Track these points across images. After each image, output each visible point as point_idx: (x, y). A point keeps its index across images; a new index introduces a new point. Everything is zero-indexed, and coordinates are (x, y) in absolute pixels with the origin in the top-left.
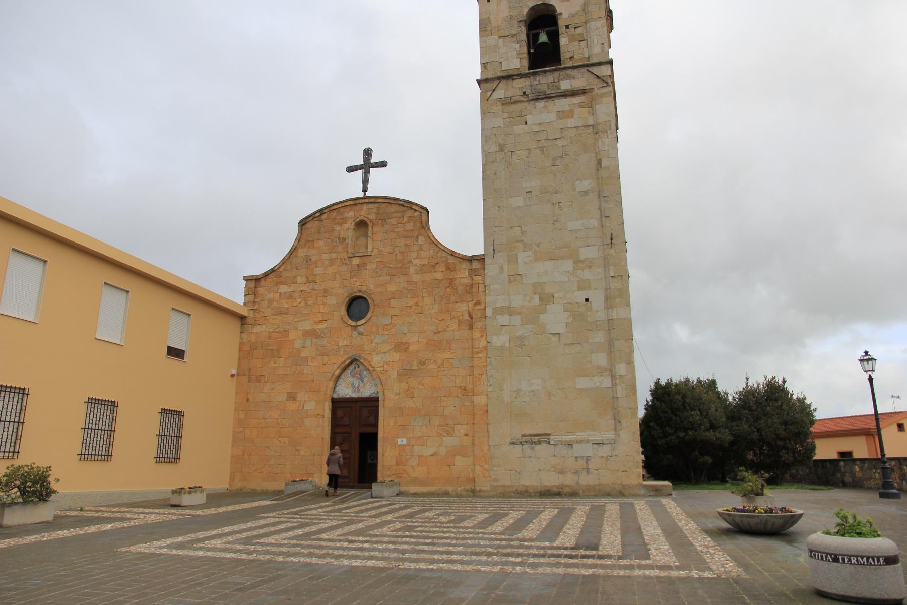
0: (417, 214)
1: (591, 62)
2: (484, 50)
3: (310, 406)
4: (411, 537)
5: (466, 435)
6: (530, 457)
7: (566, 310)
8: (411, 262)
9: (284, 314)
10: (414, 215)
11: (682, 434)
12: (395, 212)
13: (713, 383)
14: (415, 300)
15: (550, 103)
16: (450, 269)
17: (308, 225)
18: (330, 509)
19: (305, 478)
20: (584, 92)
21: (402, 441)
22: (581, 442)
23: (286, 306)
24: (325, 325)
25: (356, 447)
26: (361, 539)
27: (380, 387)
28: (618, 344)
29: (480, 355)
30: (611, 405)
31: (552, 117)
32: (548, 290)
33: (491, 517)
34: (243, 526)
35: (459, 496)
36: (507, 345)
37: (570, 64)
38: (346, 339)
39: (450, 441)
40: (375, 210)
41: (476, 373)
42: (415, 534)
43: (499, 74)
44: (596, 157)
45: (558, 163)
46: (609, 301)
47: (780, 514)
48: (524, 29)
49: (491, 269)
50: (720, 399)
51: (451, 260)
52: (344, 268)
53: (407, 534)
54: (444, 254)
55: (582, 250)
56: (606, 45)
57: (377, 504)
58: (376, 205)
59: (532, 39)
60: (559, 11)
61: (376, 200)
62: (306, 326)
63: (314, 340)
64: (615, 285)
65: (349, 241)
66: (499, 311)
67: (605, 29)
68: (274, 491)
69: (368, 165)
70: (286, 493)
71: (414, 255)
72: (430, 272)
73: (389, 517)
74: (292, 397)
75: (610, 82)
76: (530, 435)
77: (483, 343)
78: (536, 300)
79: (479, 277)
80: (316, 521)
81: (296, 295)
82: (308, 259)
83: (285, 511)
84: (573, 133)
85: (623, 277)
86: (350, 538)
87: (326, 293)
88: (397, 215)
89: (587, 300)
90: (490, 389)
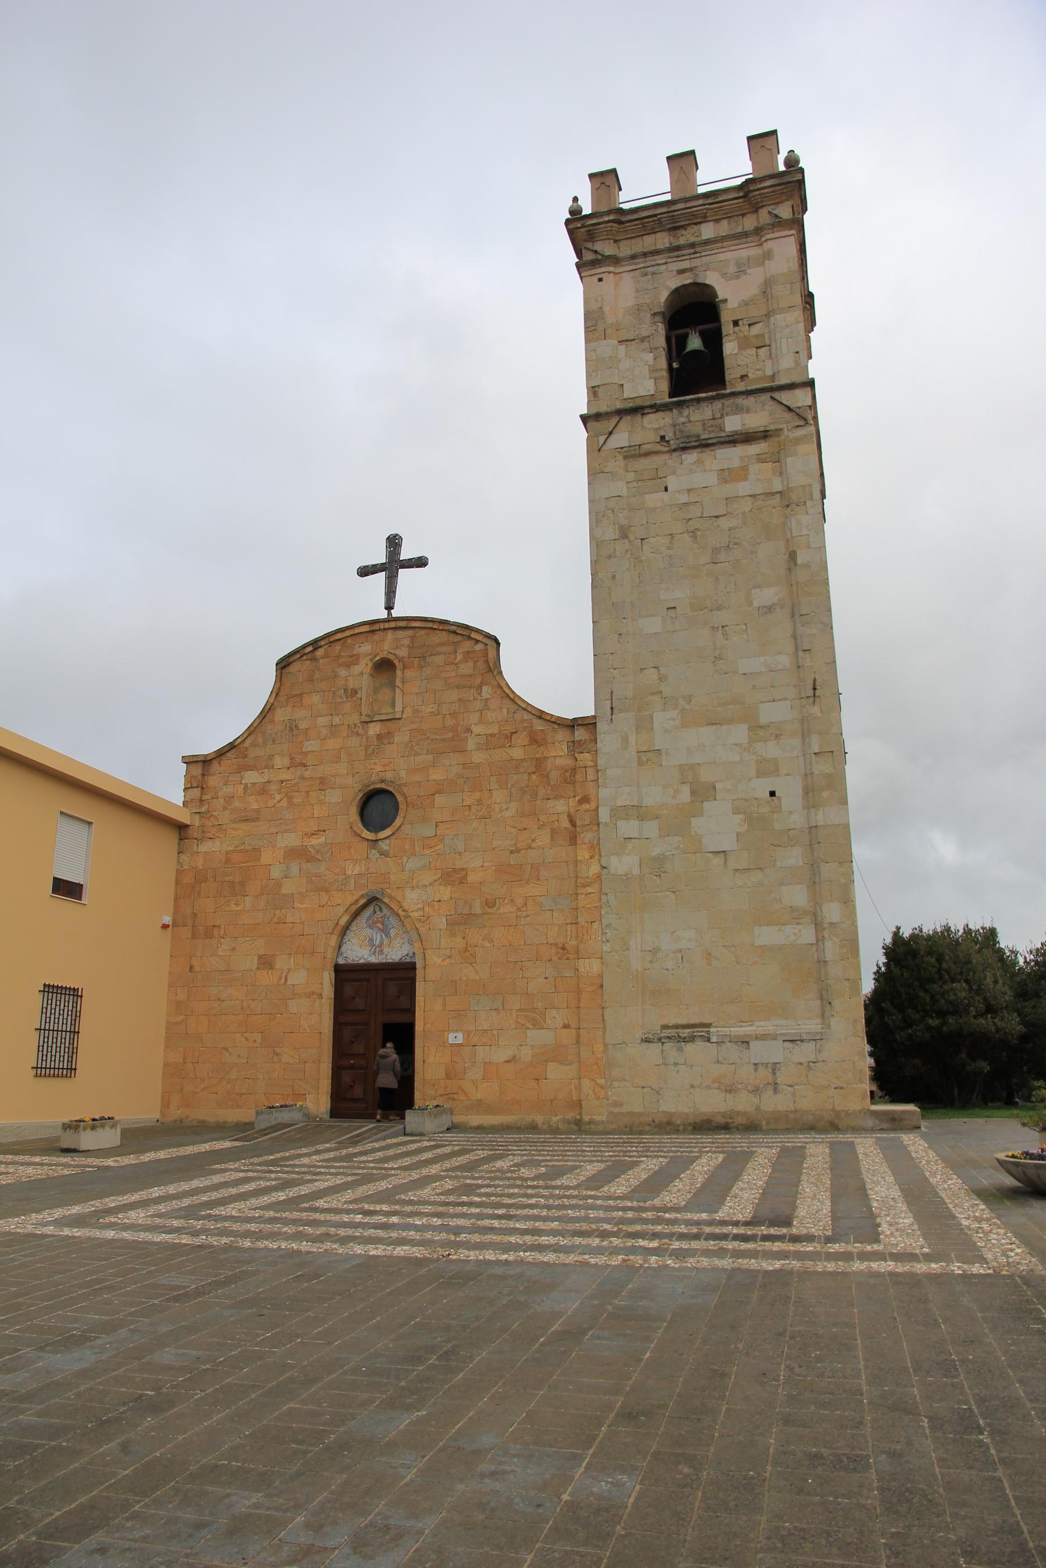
0: (479, 647)
1: (777, 383)
2: (593, 364)
4: (471, 1204)
5: (566, 1026)
6: (676, 1064)
7: (736, 811)
8: (469, 730)
9: (253, 820)
10: (472, 649)
12: (442, 644)
13: (991, 934)
15: (707, 455)
17: (293, 668)
18: (332, 1155)
19: (289, 1102)
21: (455, 1038)
22: (762, 1037)
23: (255, 806)
24: (323, 839)
27: (417, 945)
28: (827, 870)
29: (589, 890)
31: (712, 479)
34: (185, 1186)
35: (555, 1131)
36: (636, 871)
37: (741, 387)
38: (358, 864)
39: (537, 1037)
40: (407, 642)
41: (581, 920)
42: (477, 1199)
43: (619, 406)
45: (722, 557)
49: (607, 741)
50: (1003, 960)
51: (539, 725)
52: (355, 741)
53: (465, 1198)
56: (803, 354)
58: (410, 633)
59: (675, 346)
60: (721, 295)
61: (408, 623)
62: (291, 840)
64: (821, 767)
66: (622, 812)
67: (801, 327)
69: (394, 563)
70: (257, 1128)
71: (474, 717)
73: (434, 1169)
74: (266, 962)
76: (677, 1027)
77: (594, 869)
81: (273, 787)
82: (292, 727)
83: (256, 1160)
84: (747, 506)
85: (836, 753)
86: (366, 1206)
87: (323, 783)
88: (445, 649)
89: (772, 794)
90: (606, 948)
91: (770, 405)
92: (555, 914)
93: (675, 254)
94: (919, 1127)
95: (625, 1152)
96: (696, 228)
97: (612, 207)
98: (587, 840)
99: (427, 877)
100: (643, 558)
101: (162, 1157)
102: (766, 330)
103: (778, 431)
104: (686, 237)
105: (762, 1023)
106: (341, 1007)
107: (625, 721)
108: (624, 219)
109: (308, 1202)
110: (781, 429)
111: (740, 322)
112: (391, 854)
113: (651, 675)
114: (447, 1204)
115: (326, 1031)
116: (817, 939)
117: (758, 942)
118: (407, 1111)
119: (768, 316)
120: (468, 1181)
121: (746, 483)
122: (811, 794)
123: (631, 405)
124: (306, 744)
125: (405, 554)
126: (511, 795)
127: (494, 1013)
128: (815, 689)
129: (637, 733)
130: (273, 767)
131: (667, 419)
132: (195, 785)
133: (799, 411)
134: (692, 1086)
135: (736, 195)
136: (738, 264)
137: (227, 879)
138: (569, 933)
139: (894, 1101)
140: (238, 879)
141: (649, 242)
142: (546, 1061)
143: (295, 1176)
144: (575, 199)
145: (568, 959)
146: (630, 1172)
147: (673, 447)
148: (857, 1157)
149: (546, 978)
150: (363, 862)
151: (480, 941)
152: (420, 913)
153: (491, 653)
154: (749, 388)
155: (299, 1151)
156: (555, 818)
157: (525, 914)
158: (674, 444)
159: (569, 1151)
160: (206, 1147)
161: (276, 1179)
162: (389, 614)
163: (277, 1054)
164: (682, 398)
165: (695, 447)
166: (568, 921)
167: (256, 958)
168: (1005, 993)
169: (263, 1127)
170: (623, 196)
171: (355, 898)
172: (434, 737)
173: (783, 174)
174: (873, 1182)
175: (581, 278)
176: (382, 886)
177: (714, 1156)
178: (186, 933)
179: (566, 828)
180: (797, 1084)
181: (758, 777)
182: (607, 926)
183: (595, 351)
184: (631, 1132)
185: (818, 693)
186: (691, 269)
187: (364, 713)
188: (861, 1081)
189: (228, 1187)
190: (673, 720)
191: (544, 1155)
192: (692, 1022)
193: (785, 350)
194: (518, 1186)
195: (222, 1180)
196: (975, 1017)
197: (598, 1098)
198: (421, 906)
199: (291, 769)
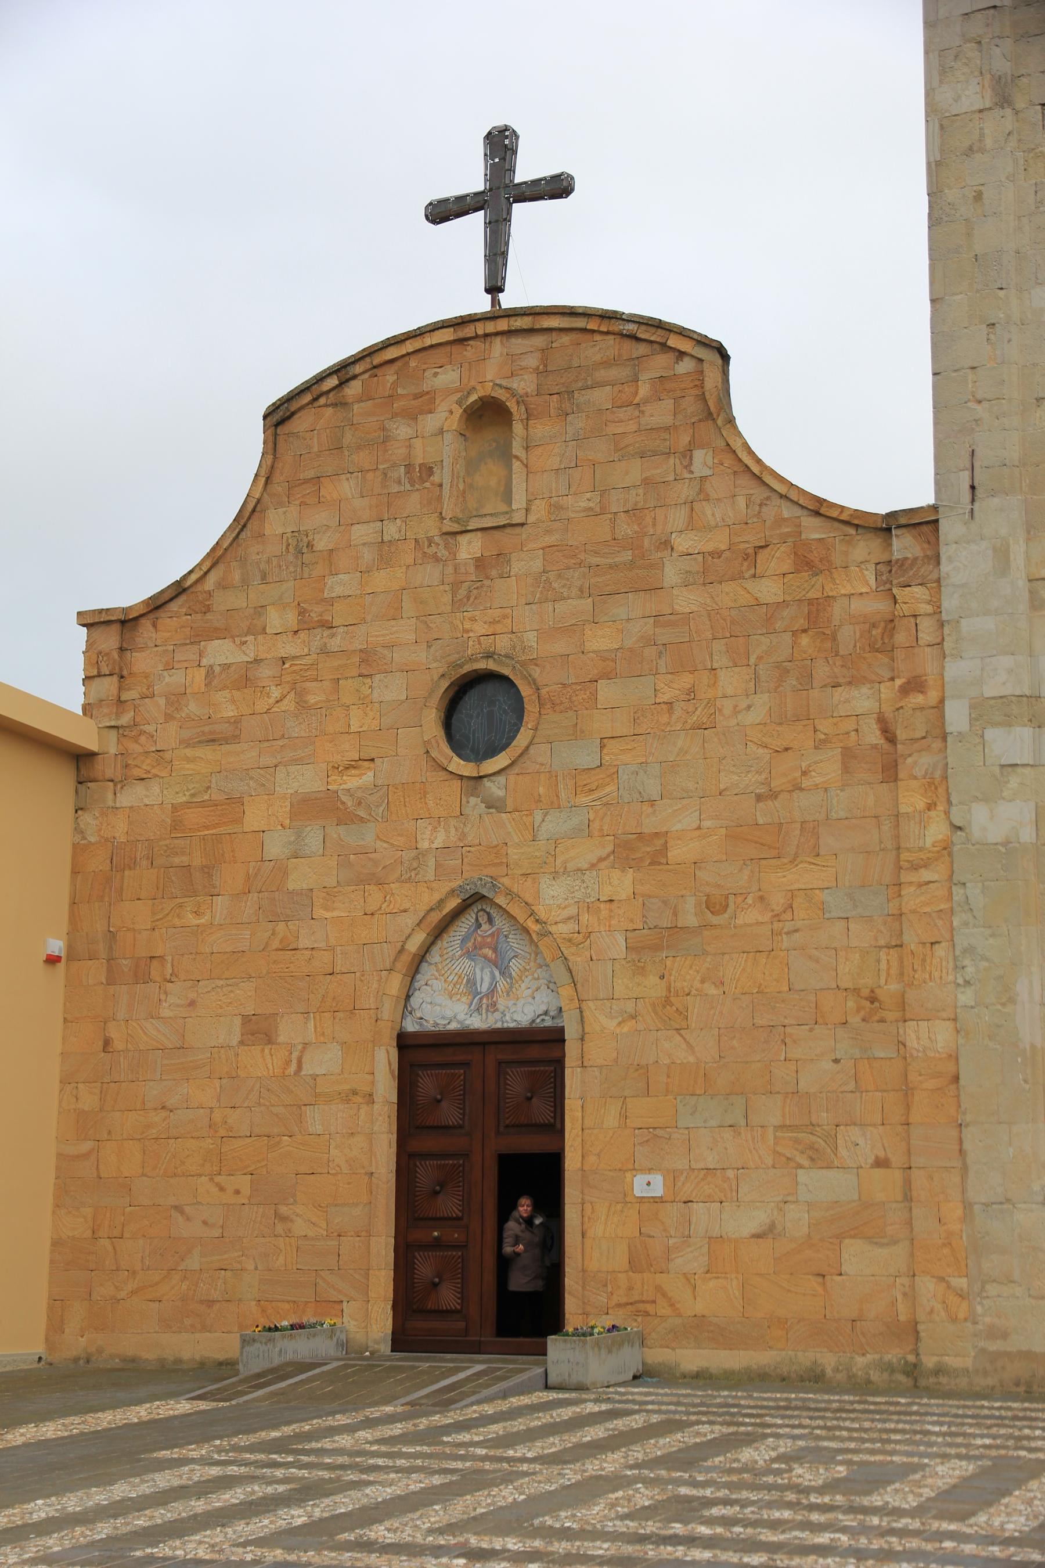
0: (685, 366)
3: (324, 1062)
4: (691, 1541)
5: (881, 1163)
8: (666, 545)
9: (226, 741)
10: (679, 370)
12: (606, 364)
14: (686, 680)
16: (809, 565)
17: (300, 424)
18: (397, 1429)
19: (308, 1318)
21: (648, 1185)
23: (230, 712)
24: (368, 777)
25: (484, 1211)
26: (512, 1544)
27: (567, 992)
29: (926, 875)
33: (983, 1472)
34: (99, 1497)
35: (862, 1387)
36: (1027, 835)
38: (444, 827)
39: (821, 1185)
40: (532, 361)
42: (704, 1530)
49: (963, 560)
51: (814, 530)
52: (429, 574)
53: (678, 1528)
54: (787, 511)
57: (566, 1413)
58: (539, 341)
61: (535, 321)
62: (306, 780)
63: (333, 832)
65: (443, 475)
66: (992, 711)
68: (202, 1364)
69: (502, 191)
70: (244, 1372)
71: (678, 517)
73: (610, 1463)
74: (259, 1030)
77: (936, 831)
80: (352, 1476)
81: (265, 672)
82: (301, 546)
83: (243, 1440)
86: (473, 1541)
87: (368, 663)
88: (613, 373)
90: (966, 997)
92: (852, 926)
95: (1020, 1438)
98: (919, 772)
99: (586, 852)
101: (50, 1435)
106: (412, 1119)
107: (1002, 515)
109: (352, 1530)
114: (643, 1539)
115: (383, 1171)
118: (551, 1339)
120: (684, 1490)
124: (330, 581)
125: (525, 171)
126: (756, 677)
127: (728, 1134)
129: (1028, 540)
130: (264, 631)
132: (105, 670)
137: (177, 860)
138: (883, 965)
140: (198, 861)
142: (840, 1237)
143: (326, 1474)
145: (882, 1021)
146: (1033, 1484)
149: (836, 1061)
150: (453, 822)
151: (697, 984)
152: (572, 926)
155: (330, 1421)
156: (850, 725)
157: (788, 926)
159: (895, 1431)
160: (141, 1413)
161: (285, 1481)
162: (495, 302)
163: (284, 1219)
166: (882, 942)
167: (238, 1021)
169: (257, 1370)
171: (437, 897)
172: (595, 560)
176: (492, 871)
178: (94, 972)
179: (874, 747)
182: (965, 951)
184: (1029, 1396)
187: (448, 514)
189: (188, 1497)
191: (842, 1440)
194: (790, 1505)
195: (176, 1482)
197: (954, 1320)
198: (572, 911)
199: (302, 635)
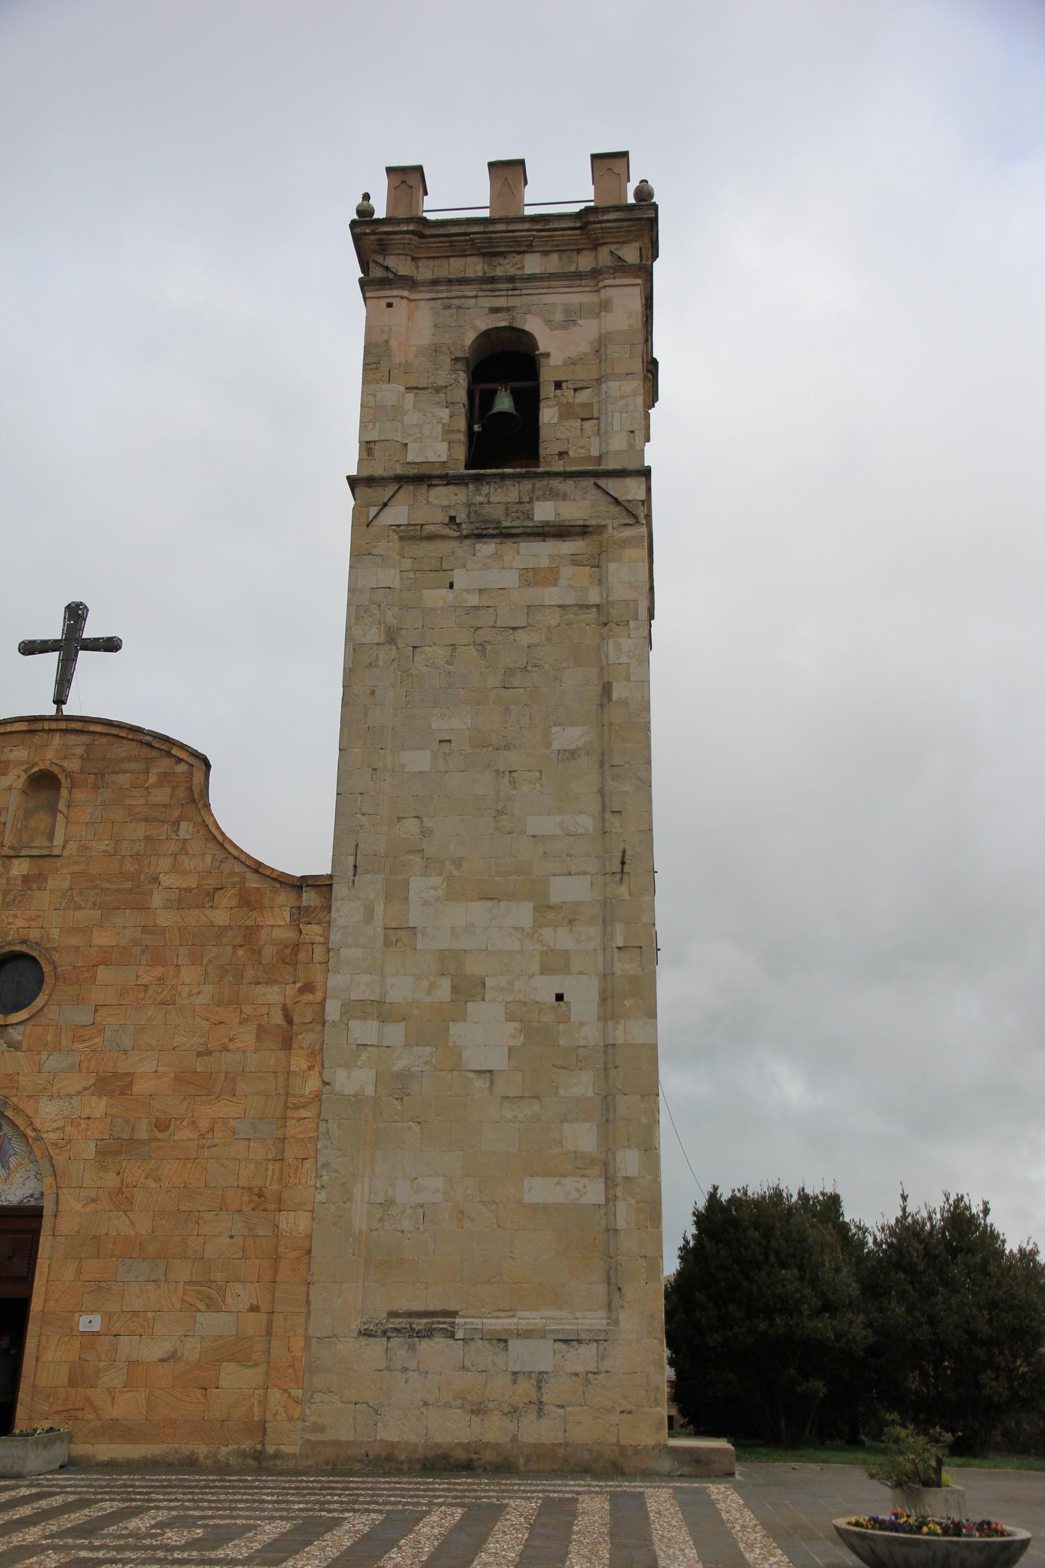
0: (181, 768)
1: (605, 466)
2: (371, 412)
6: (405, 1369)
7: (510, 1018)
8: (156, 880)
10: (173, 771)
11: (762, 1326)
13: (833, 1202)
14: (159, 971)
15: (508, 548)
20: (583, 531)
21: (89, 1322)
22: (527, 1334)
27: (49, 1181)
28: (626, 1105)
29: (303, 1113)
30: (602, 1246)
31: (511, 579)
32: (473, 968)
33: (297, 1528)
35: (222, 1469)
36: (369, 1091)
37: (558, 466)
39: (213, 1324)
40: (80, 751)
41: (289, 1155)
43: (399, 470)
44: (601, 675)
45: (516, 681)
46: (608, 999)
47: (977, 1538)
48: (463, 379)
49: (345, 911)
50: (846, 1238)
51: (253, 882)
54: (238, 868)
55: (556, 883)
56: (640, 435)
58: (85, 739)
59: (479, 404)
60: (543, 346)
61: (84, 725)
64: (625, 967)
66: (356, 1009)
67: (640, 400)
69: (73, 641)
71: (165, 863)
72: (202, 906)
73: (31, 1535)
75: (642, 515)
76: (409, 1314)
77: (313, 1084)
78: (444, 991)
79: (315, 927)
84: (553, 619)
85: (644, 949)
88: (133, 766)
89: (559, 997)
90: (321, 1196)
91: (594, 494)
93: (489, 286)
94: (733, 1474)
96: (518, 258)
97: (413, 214)
98: (306, 1044)
99: (75, 1083)
100: (414, 672)
102: (595, 399)
103: (601, 528)
104: (504, 267)
105: (527, 1314)
108: (427, 232)
110: (605, 526)
111: (564, 385)
112: (25, 1047)
113: (412, 826)
116: (607, 1197)
117: (528, 1199)
119: (599, 381)
120: (83, 1554)
121: (555, 589)
122: (609, 1000)
123: (415, 471)
125: (89, 632)
126: (206, 974)
127: (151, 1286)
128: (623, 863)
129: (386, 903)
131: (460, 496)
133: (629, 506)
134: (426, 1404)
135: (571, 225)
136: (567, 311)
139: (699, 1433)
141: (456, 267)
144: (366, 197)
145: (265, 1210)
147: (465, 533)
148: (648, 1518)
149: (232, 1237)
151: (142, 1180)
153: (198, 778)
154: (568, 469)
157: (210, 1142)
158: (466, 529)
162: (59, 710)
164: (482, 471)
165: (493, 536)
166: (270, 1157)
168: (848, 1286)
170: (428, 203)
172: (106, 885)
173: (632, 206)
174: (668, 1557)
175: (365, 299)
177: (449, 1511)
179: (279, 1026)
180: (570, 1405)
181: (541, 973)
182: (324, 1165)
183: (375, 396)
184: (333, 1472)
185: (627, 869)
186: (508, 309)
188: (657, 1405)
190: (436, 889)
191: (203, 1509)
192: (431, 1308)
193: (617, 427)
196: (810, 1317)
198: (60, 1124)
